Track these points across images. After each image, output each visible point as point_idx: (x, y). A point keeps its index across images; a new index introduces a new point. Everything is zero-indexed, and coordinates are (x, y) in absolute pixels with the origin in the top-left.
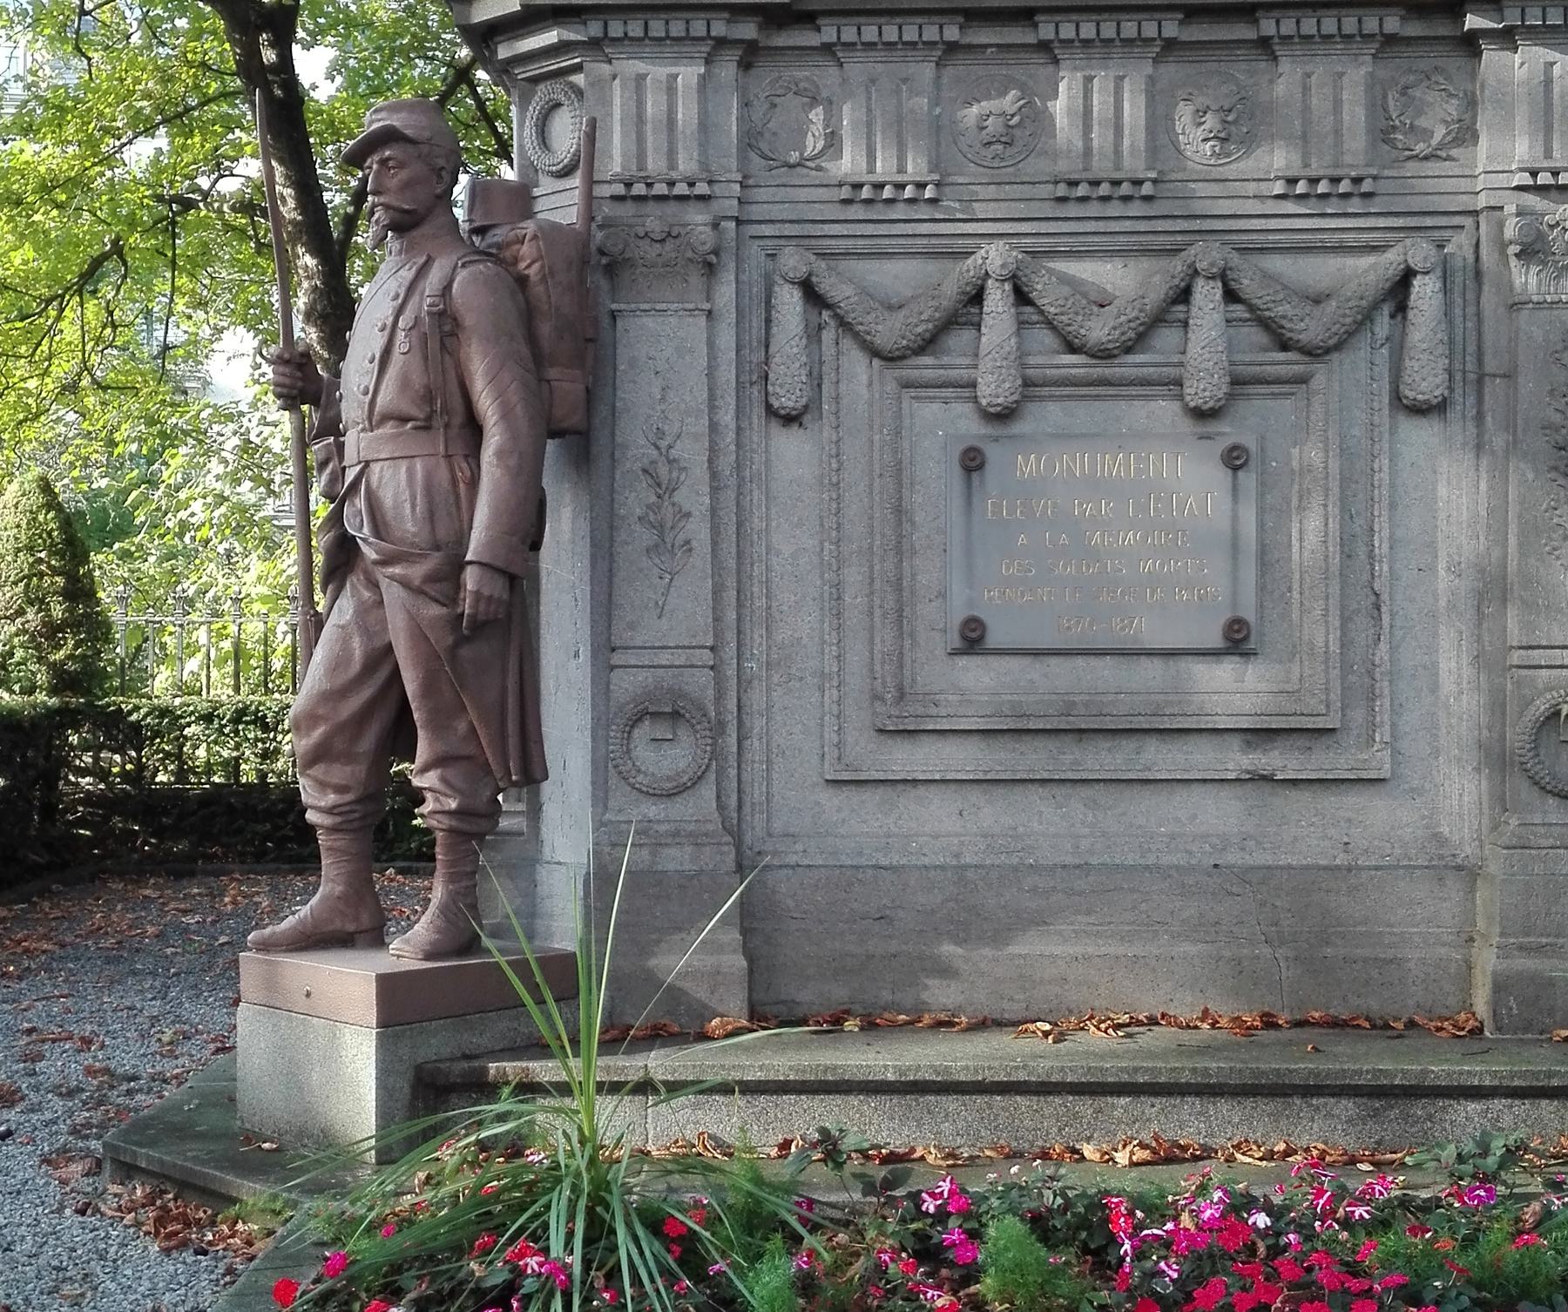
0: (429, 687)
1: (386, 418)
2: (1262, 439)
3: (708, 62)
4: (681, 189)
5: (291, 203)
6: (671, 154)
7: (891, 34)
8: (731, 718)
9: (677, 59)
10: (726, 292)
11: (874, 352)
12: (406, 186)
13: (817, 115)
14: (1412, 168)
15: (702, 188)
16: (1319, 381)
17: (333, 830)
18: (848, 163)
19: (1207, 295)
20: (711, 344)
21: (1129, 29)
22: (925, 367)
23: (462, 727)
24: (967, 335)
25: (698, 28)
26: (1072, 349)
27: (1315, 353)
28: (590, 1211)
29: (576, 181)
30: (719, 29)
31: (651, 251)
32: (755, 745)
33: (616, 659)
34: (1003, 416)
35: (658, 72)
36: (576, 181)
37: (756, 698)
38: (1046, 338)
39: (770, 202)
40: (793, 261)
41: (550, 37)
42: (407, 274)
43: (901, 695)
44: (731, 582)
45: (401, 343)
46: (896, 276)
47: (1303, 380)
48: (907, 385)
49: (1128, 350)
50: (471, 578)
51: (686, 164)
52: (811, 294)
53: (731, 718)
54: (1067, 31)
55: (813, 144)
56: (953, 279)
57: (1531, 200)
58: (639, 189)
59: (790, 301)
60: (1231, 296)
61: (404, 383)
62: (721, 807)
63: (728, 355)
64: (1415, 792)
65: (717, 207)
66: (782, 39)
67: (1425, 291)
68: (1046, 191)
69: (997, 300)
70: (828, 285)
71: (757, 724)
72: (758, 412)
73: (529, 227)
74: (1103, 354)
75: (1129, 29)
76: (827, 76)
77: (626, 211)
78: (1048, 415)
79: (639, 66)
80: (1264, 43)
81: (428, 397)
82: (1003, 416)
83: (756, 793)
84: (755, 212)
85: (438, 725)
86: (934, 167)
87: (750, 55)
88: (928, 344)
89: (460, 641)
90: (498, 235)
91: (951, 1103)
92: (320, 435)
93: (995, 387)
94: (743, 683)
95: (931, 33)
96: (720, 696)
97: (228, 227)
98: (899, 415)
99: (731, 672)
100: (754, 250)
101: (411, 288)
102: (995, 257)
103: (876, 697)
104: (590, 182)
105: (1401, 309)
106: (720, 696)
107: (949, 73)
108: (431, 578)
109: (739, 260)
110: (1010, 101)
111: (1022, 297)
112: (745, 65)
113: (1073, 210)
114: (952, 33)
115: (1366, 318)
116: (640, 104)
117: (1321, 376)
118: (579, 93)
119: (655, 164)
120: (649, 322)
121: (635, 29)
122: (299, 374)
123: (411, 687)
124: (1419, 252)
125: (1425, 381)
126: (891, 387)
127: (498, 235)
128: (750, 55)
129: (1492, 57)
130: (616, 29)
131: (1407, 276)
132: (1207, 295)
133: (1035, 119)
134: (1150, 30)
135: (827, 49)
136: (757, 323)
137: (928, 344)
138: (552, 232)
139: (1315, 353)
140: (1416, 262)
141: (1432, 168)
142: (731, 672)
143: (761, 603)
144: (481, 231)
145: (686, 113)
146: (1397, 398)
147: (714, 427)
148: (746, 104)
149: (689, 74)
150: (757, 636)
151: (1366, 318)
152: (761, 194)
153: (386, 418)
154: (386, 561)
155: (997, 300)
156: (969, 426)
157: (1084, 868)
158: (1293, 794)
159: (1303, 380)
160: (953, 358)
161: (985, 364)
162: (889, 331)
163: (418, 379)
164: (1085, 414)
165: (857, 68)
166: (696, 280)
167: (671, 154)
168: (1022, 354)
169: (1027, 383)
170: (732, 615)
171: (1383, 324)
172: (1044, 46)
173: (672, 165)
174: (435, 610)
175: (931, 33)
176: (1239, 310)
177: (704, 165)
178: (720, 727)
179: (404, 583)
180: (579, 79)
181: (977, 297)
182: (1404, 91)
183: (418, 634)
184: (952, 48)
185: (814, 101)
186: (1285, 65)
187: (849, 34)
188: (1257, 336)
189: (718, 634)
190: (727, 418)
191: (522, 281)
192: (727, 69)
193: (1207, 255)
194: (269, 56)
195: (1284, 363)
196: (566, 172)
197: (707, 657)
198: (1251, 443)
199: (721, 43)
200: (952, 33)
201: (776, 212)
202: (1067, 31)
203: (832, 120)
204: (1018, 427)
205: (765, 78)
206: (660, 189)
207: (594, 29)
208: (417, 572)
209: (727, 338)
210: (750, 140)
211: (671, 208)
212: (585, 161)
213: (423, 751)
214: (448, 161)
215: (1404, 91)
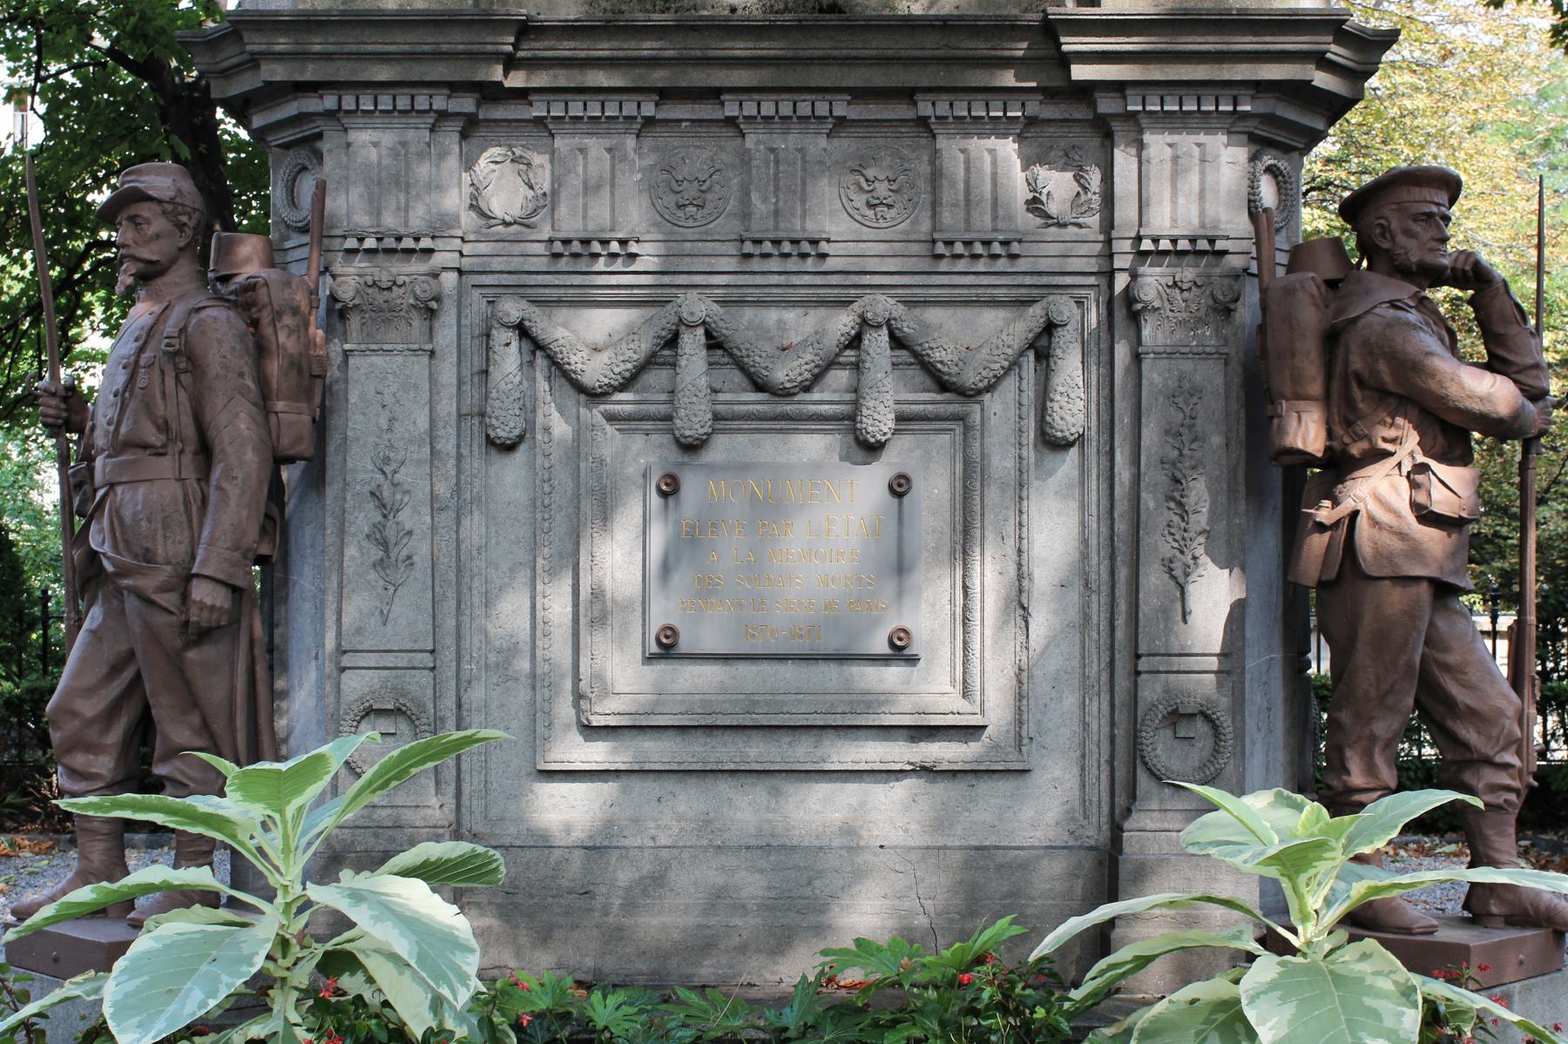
10: (446, 335)
15: (426, 243)
20: (432, 379)
30: (440, 103)
45: (185, 937)
66: (499, 112)
75: (804, 109)
95: (630, 109)
107: (648, 142)
112: (464, 136)
113: (756, 265)
114: (649, 109)
122: (63, 406)
134: (822, 109)
137: (627, 384)
142: (450, 672)
169: (717, 417)
181: (672, 341)
184: (649, 122)
199: (443, 115)
214: (190, 218)
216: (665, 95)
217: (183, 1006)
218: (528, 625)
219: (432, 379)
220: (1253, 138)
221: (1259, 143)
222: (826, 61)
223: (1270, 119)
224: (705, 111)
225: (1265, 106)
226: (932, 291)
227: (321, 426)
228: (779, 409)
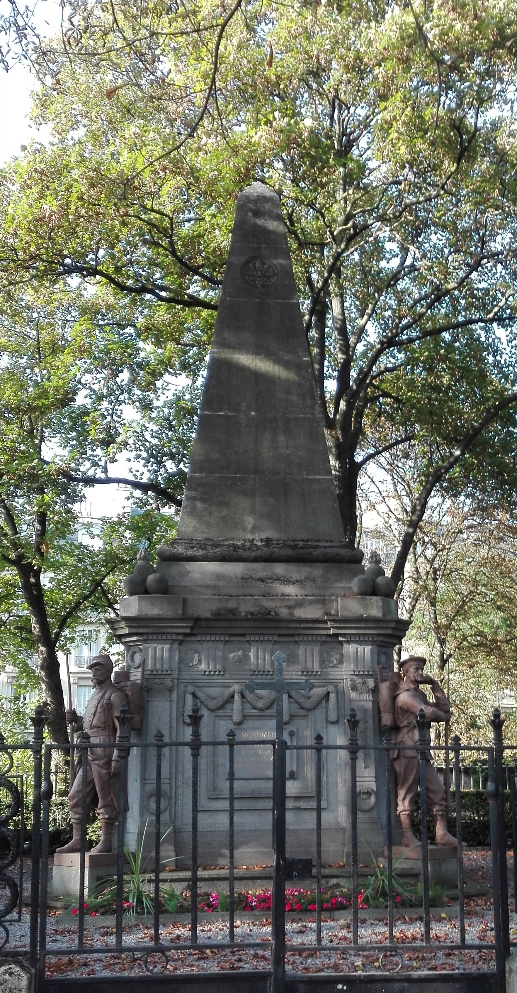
0: (102, 790)
1: (94, 727)
2: (298, 729)
3: (171, 644)
4: (164, 672)
5: (37, 630)
6: (162, 664)
7: (213, 638)
8: (173, 795)
9: (164, 644)
10: (174, 696)
11: (209, 709)
12: (100, 675)
13: (196, 656)
14: (329, 669)
15: (169, 672)
16: (310, 716)
17: (76, 824)
18: (203, 667)
20: (171, 708)
21: (266, 638)
22: (220, 713)
23: (109, 798)
24: (231, 705)
25: (169, 637)
26: (255, 708)
27: (309, 710)
28: (138, 899)
29: (140, 670)
31: (157, 687)
32: (179, 802)
33: (147, 782)
34: (239, 724)
35: (159, 647)
36: (140, 670)
37: (180, 791)
38: (249, 706)
39: (185, 674)
40: (190, 689)
41: (135, 638)
42: (100, 694)
43: (214, 790)
44: (174, 763)
45: (99, 710)
46: (214, 691)
47: (307, 716)
48: (216, 716)
49: (267, 709)
50: (113, 764)
51: (166, 667)
52: (194, 695)
53: (173, 795)
54: (253, 638)
55: (195, 662)
56: (227, 693)
57: (355, 677)
58: (155, 672)
59: (189, 698)
60: (290, 697)
61: (99, 719)
62: (170, 817)
63: (175, 710)
64: (333, 811)
65: (172, 677)
66: (188, 639)
67: (332, 696)
68: (248, 673)
69: (237, 697)
70: (198, 694)
71: (180, 797)
72: (181, 724)
73: (129, 683)
74: (261, 710)
76: (199, 647)
77: (152, 677)
78: (250, 723)
79: (156, 645)
80: (296, 642)
81: (105, 723)
82: (239, 724)
83: (179, 814)
84: (182, 677)
85: (104, 797)
86: (223, 667)
87: (181, 643)
88: (222, 707)
89: (110, 778)
90: (122, 684)
91: (220, 883)
92: (77, 731)
94: (177, 787)
96: (171, 790)
97: (11, 633)
98: (214, 724)
99: (174, 785)
100: (182, 685)
101: (102, 697)
102: (236, 688)
103: (208, 790)
104: (143, 671)
105: (328, 700)
106: (171, 790)
107: (226, 646)
108: (104, 764)
109: (178, 688)
110: (240, 653)
111: (243, 696)
114: (227, 638)
115: (320, 702)
116: (155, 653)
117: (311, 715)
118: (141, 650)
119: (158, 666)
120: (156, 703)
121: (155, 637)
123: (98, 789)
124: (331, 688)
125: (333, 716)
126: (213, 717)
127: (122, 684)
128: (181, 643)
129: (345, 646)
130: (150, 637)
131: (328, 693)
133: (247, 657)
134: (271, 638)
135: (199, 641)
136: (182, 702)
137: (222, 707)
138: (134, 684)
139: (309, 710)
140: (330, 690)
141: (333, 669)
142: (174, 785)
143: (181, 768)
144: (118, 683)
145: (166, 655)
146: (327, 721)
147: (171, 727)
148: (180, 653)
149: (167, 647)
150: (180, 776)
151: (320, 702)
152: (183, 673)
153: (94, 727)
154: (94, 760)
155: (237, 697)
156: (231, 726)
157: (257, 831)
158: (305, 812)
159: (307, 716)
160: (227, 712)
161: (234, 712)
162: (212, 704)
163: (102, 718)
164: (257, 723)
165: (206, 645)
166: (167, 694)
167: (162, 664)
168: (243, 709)
169: (244, 716)
170: (294, 625)
171: (324, 702)
172: (248, 641)
173: (162, 667)
174: (105, 771)
175: (222, 638)
176: (292, 700)
177: (170, 667)
178: (170, 798)
179: (98, 765)
180: (141, 647)
181: (233, 696)
182: (328, 652)
183: (100, 776)
184: (227, 641)
185: (196, 652)
186: (301, 647)
187: (204, 638)
188: (296, 706)
189: (171, 775)
190: (174, 724)
191: (127, 695)
192: (176, 645)
194: (32, 580)
195: (301, 712)
196: (138, 667)
197: (168, 781)
198: (295, 730)
199: (174, 640)
200: (227, 638)
201: (187, 677)
202: (253, 638)
203: (200, 656)
204: (244, 726)
205: (184, 647)
206: (160, 672)
207: (145, 637)
208: (101, 762)
209: (174, 706)
210: (181, 661)
211: (162, 677)
212: (143, 664)
213: (100, 804)
215: (328, 652)
216: (231, 635)
217: (208, 50)
218: (78, 887)
219: (171, 708)
220: (378, 646)
222: (271, 628)
223: (382, 641)
224: (241, 639)
225: (380, 639)
226: (363, 625)
227: (142, 720)
228: (263, 714)
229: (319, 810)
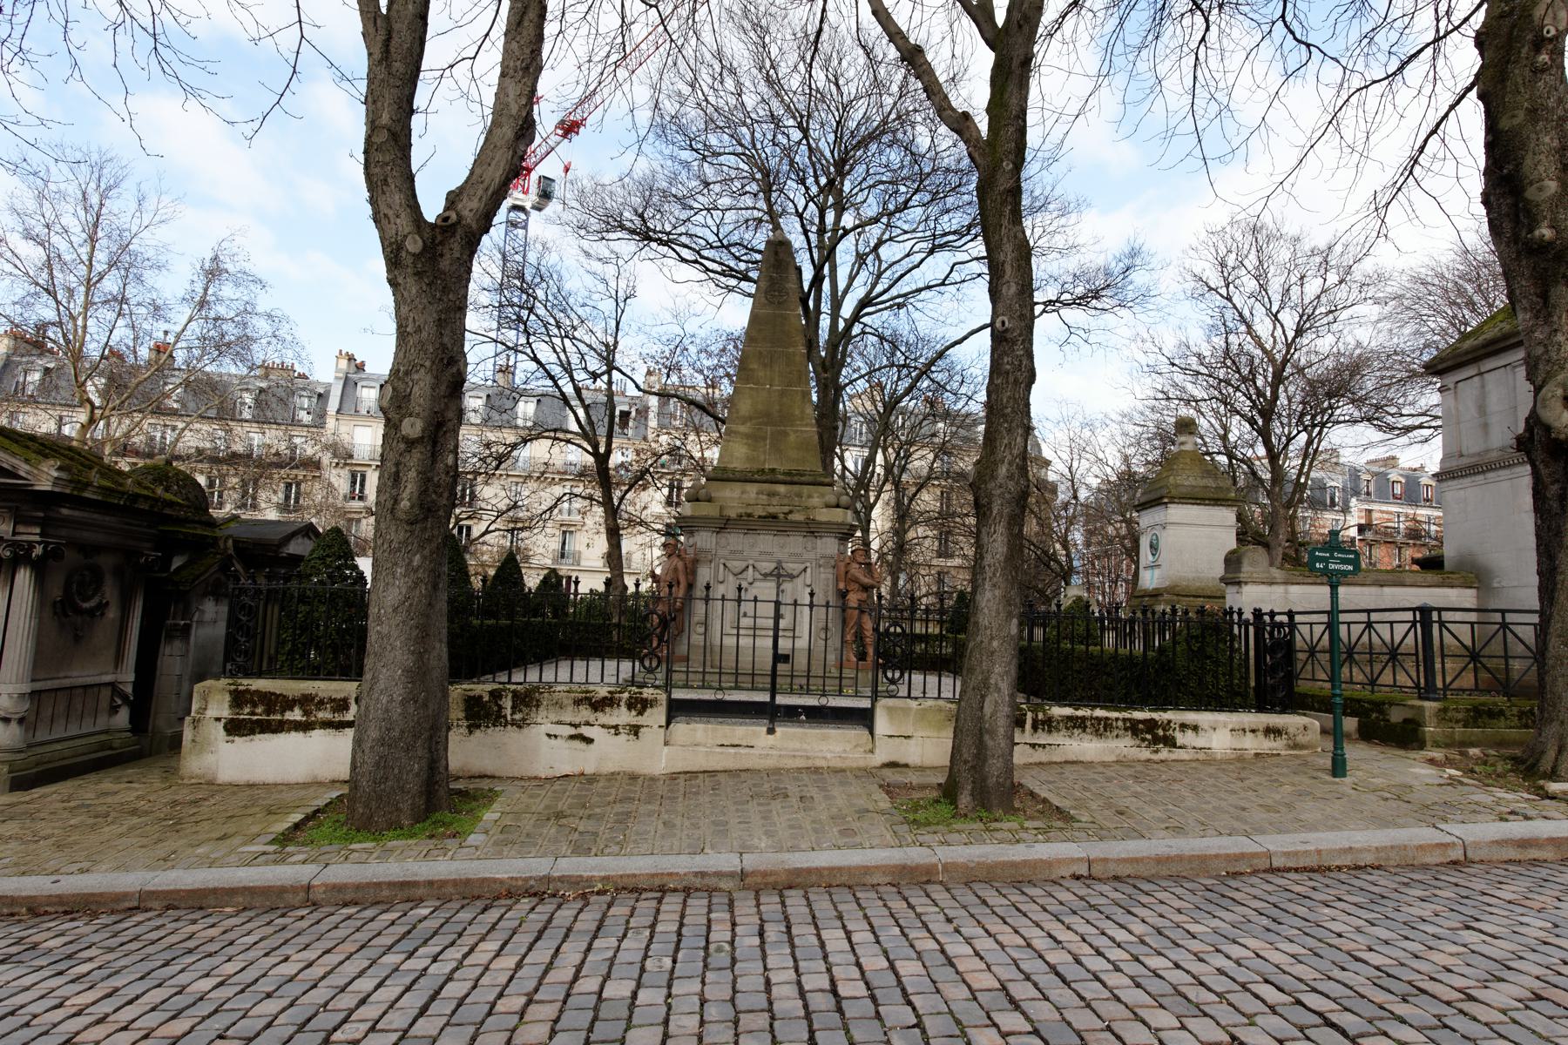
19: (751, 568)
59: (722, 567)
67: (809, 570)
93: (750, 580)
132: (751, 568)
193: (751, 562)
221: (840, 539)
229: (794, 637)
